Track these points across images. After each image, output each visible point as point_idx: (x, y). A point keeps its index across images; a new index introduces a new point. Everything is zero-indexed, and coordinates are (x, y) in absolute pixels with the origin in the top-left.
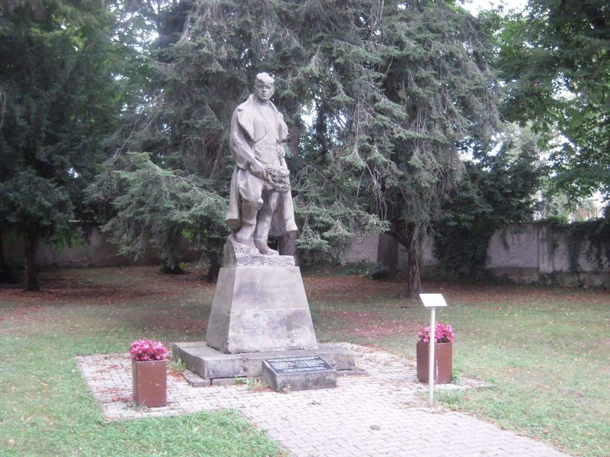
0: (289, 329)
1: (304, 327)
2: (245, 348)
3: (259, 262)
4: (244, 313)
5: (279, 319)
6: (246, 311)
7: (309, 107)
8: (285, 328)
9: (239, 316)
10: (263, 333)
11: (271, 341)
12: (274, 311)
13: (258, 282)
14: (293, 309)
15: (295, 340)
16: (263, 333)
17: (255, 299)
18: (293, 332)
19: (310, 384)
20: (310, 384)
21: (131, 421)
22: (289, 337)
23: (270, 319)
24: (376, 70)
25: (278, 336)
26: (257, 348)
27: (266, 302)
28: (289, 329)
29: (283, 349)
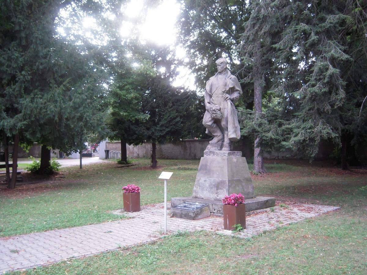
0: (217, 190)
1: (224, 189)
2: (199, 196)
3: (212, 155)
4: (201, 179)
5: (214, 183)
6: (202, 178)
7: (25, 134)
8: (216, 188)
9: (199, 180)
10: (206, 190)
11: (209, 194)
12: (212, 179)
13: (208, 164)
14: (221, 179)
15: (219, 196)
16: (206, 190)
17: (206, 173)
18: (219, 191)
19: (183, 216)
20: (183, 216)
21: (190, 229)
22: (216, 194)
23: (210, 183)
24: (275, 48)
25: (212, 193)
26: (203, 197)
27: (210, 174)
28: (217, 190)
29: (213, 199)
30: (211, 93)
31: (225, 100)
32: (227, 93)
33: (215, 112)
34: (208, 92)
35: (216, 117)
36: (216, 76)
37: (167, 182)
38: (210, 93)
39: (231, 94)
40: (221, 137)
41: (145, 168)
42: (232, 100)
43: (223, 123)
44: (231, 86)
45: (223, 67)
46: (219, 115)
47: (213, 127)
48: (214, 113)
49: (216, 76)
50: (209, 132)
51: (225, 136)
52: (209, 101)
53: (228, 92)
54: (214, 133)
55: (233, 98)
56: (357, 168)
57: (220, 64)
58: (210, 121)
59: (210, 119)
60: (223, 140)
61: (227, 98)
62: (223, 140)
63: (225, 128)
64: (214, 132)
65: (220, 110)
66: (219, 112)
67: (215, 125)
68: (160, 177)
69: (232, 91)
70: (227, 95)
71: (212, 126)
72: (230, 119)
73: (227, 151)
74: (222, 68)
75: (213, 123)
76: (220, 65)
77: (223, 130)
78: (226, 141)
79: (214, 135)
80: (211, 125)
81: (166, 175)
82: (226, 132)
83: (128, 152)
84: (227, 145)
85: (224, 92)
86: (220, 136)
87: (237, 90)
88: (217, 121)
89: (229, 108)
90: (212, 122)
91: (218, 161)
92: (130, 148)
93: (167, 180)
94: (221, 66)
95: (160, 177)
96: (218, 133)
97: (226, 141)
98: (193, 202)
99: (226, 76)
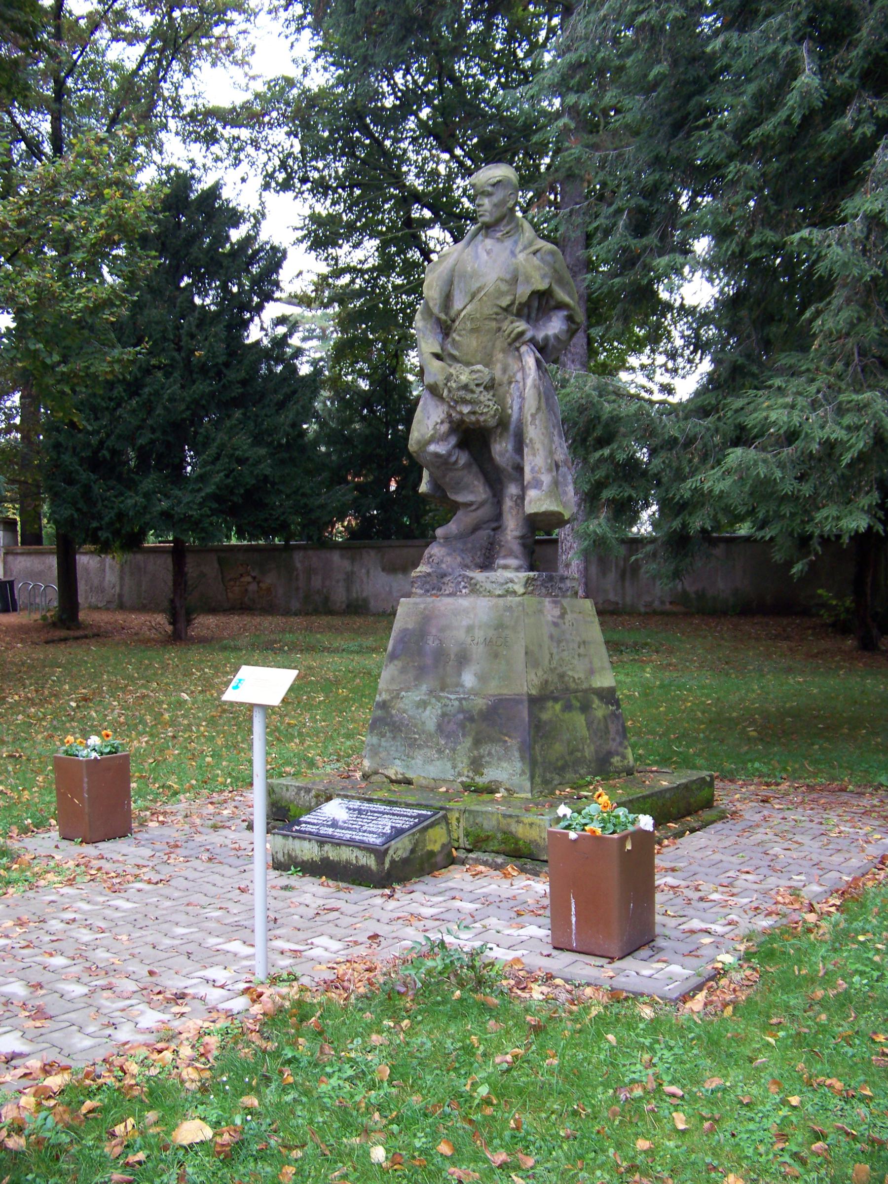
18: (484, 750)
30: (447, 314)
31: (510, 344)
32: (519, 315)
33: (469, 397)
34: (436, 310)
35: (473, 418)
36: (469, 243)
37: (267, 716)
38: (443, 317)
39: (537, 320)
40: (485, 512)
41: (146, 642)
42: (542, 348)
43: (501, 450)
44: (542, 286)
45: (503, 202)
46: (486, 408)
47: (456, 462)
48: (465, 402)
49: (469, 243)
50: (436, 485)
51: (508, 503)
52: (437, 349)
53: (526, 311)
54: (456, 493)
55: (546, 339)
56: (309, 629)
57: (489, 189)
58: (444, 438)
59: (445, 428)
60: (496, 520)
61: (521, 334)
62: (494, 525)
63: (510, 469)
64: (458, 487)
65: (491, 386)
66: (485, 397)
67: (463, 458)
68: (230, 695)
69: (538, 309)
70: (521, 325)
71: (453, 459)
72: (534, 433)
73: (518, 569)
74: (496, 206)
75: (454, 447)
76: (489, 195)
77: (495, 479)
78: (512, 528)
79: (456, 502)
80: (449, 454)
81: (261, 684)
82: (513, 490)
83: (82, 587)
84: (516, 547)
85: (506, 309)
86: (482, 504)
87: (561, 306)
88: (473, 438)
89: (529, 382)
90: (453, 440)
91: (475, 612)
92: (86, 561)
93: (264, 708)
94: (495, 199)
95: (230, 695)
96: (474, 492)
97: (512, 528)
98: (370, 800)
99: (516, 242)
